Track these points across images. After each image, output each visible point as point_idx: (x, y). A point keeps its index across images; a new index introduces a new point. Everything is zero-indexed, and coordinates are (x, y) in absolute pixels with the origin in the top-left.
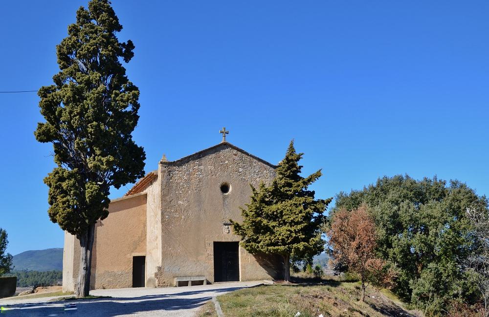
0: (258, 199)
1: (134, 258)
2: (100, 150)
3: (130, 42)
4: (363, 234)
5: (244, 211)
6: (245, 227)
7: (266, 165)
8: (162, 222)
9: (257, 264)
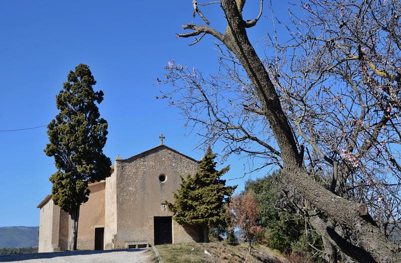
0: (185, 186)
1: (96, 229)
2: (85, 161)
3: (101, 92)
4: (249, 210)
5: (175, 194)
6: (177, 205)
7: (192, 161)
8: (117, 203)
9: (186, 232)
